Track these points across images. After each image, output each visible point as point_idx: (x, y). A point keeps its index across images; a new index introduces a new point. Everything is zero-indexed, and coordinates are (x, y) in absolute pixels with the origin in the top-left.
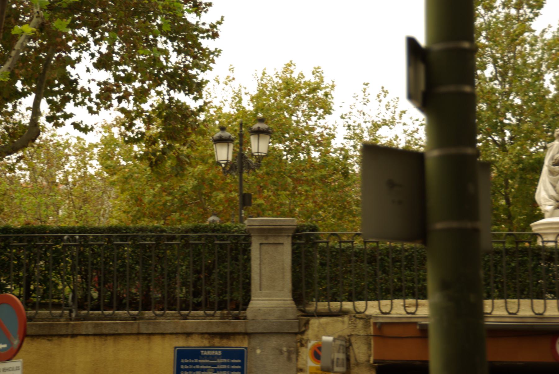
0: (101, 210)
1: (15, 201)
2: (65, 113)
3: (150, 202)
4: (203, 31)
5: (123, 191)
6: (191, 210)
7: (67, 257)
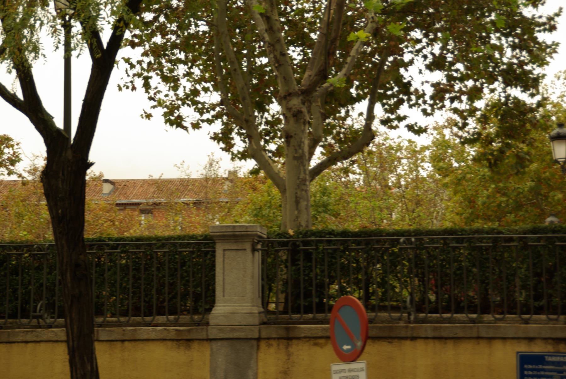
0: (433, 213)
1: (351, 205)
2: (399, 115)
3: (484, 203)
4: (539, 25)
5: (455, 193)
6: (527, 211)
7: (404, 259)
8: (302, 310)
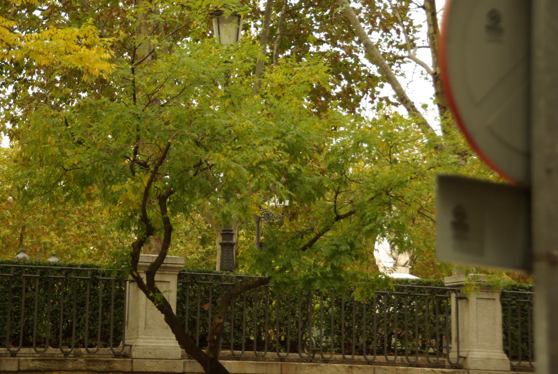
8: (232, 347)
